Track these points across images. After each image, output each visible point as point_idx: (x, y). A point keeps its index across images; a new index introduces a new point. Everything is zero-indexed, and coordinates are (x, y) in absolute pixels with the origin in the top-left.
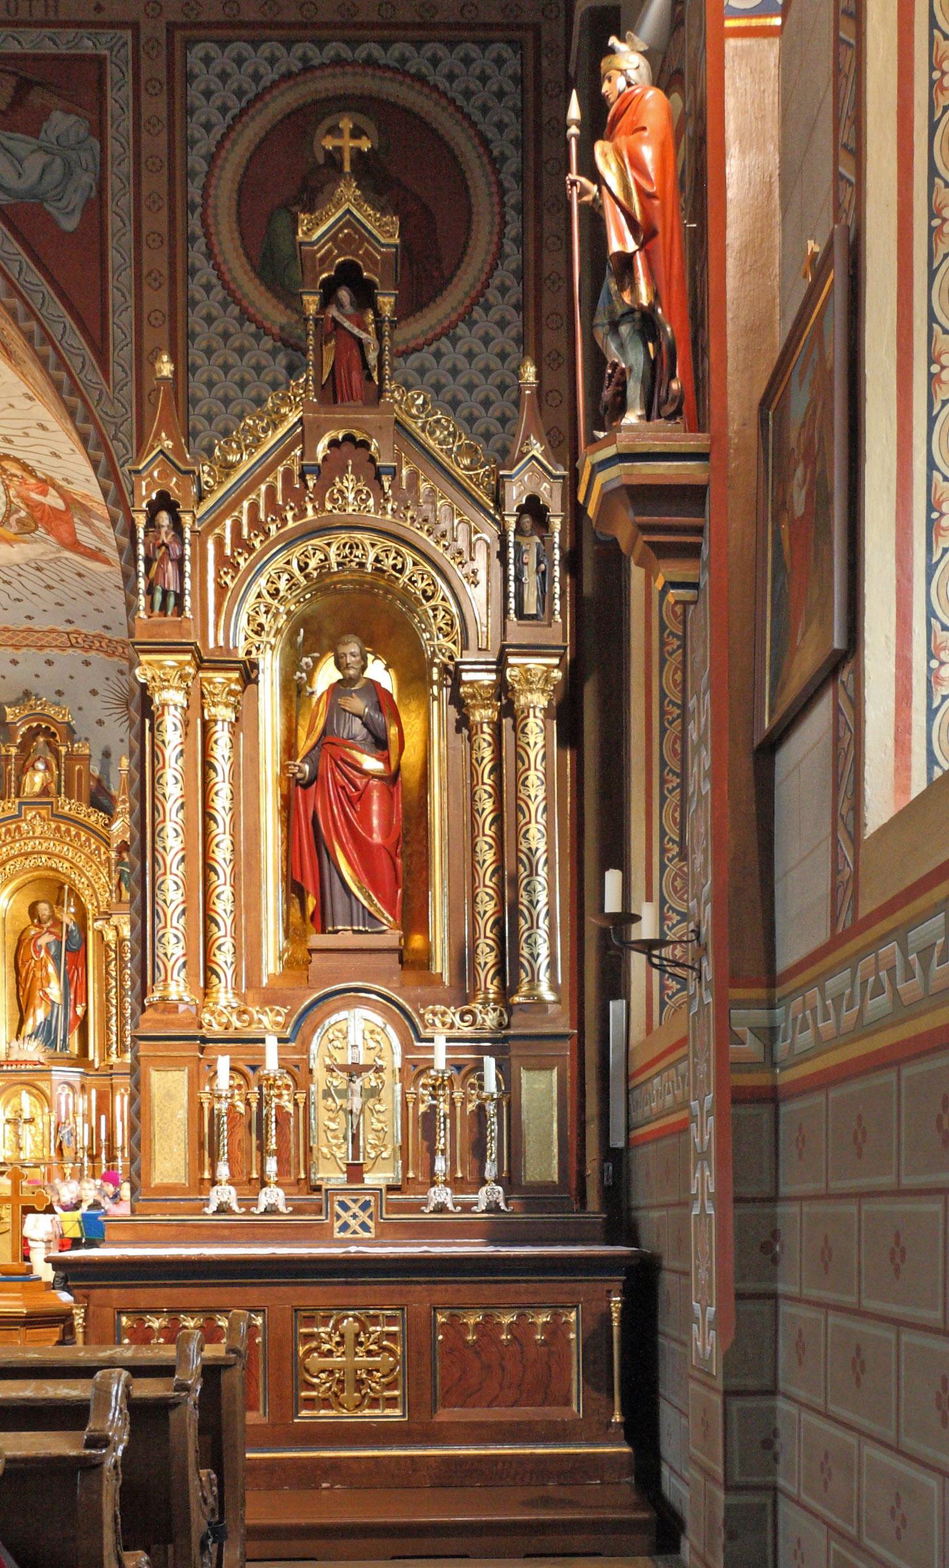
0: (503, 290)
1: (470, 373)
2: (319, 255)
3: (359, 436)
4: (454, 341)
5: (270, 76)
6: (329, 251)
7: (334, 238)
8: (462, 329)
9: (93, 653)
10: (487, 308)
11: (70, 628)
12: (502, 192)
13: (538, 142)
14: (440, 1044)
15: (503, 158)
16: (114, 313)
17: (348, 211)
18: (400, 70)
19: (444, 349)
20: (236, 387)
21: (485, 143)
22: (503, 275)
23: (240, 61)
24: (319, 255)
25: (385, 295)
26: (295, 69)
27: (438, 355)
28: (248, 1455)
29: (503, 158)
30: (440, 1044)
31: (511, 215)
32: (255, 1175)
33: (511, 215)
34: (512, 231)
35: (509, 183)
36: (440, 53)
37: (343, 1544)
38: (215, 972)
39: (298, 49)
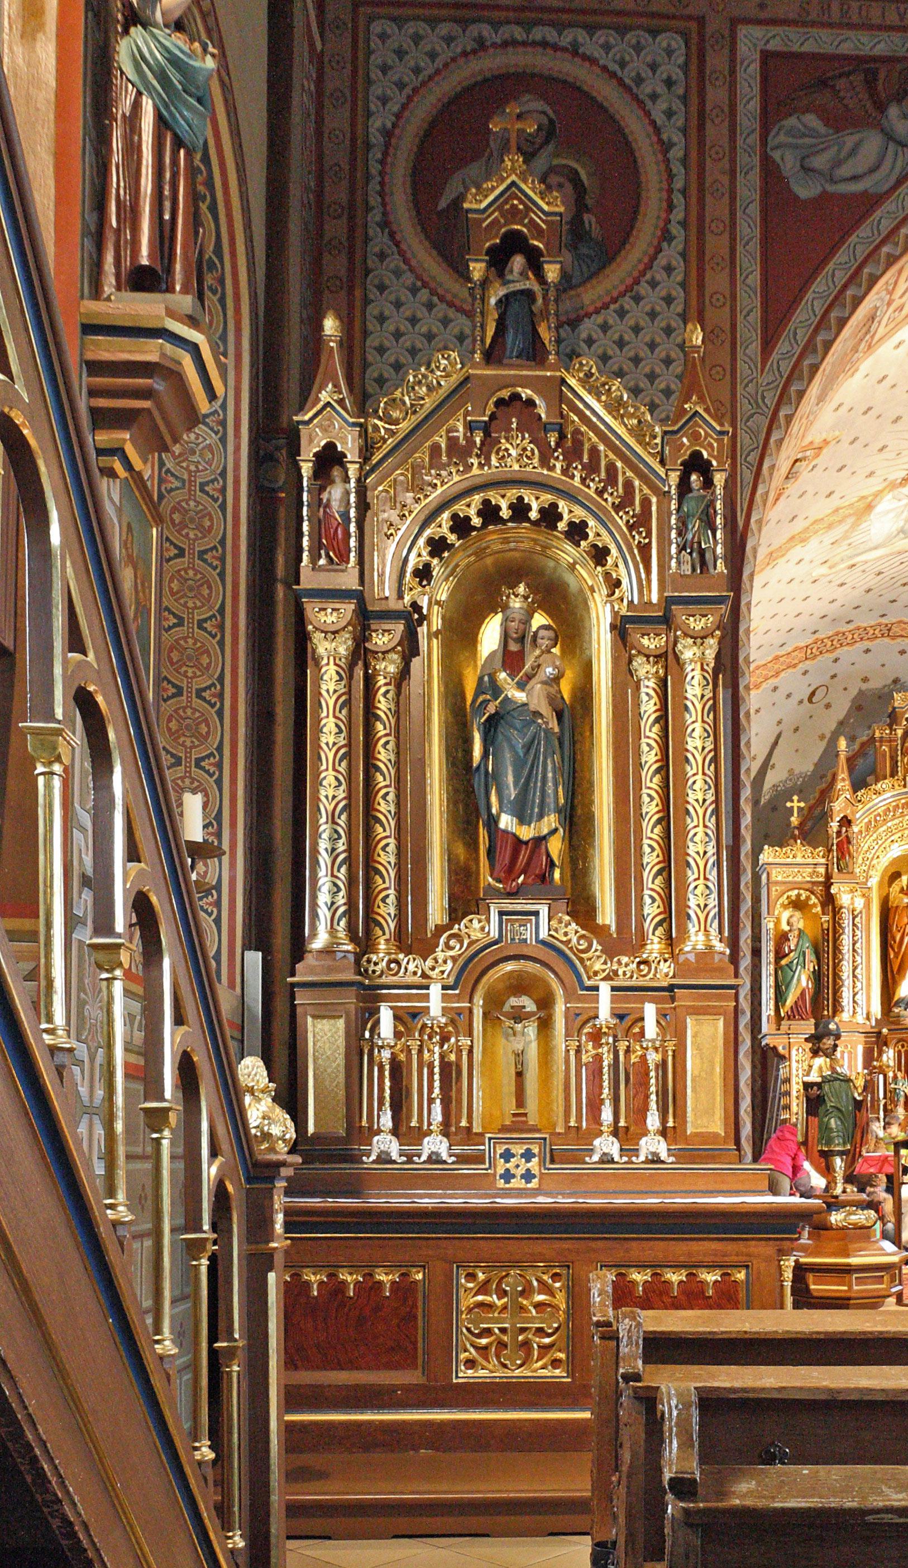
0: (669, 269)
1: (638, 345)
2: (484, 225)
3: (505, 394)
4: (637, 299)
5: (445, 54)
6: (496, 221)
7: (500, 208)
8: (627, 302)
9: (839, 651)
10: (653, 284)
11: (851, 627)
12: (671, 177)
13: (701, 127)
14: (605, 990)
15: (671, 145)
16: (850, 268)
17: (513, 183)
18: (574, 50)
19: (627, 307)
20: (646, 348)
21: (657, 130)
22: (671, 253)
23: (417, 39)
24: (484, 225)
25: (477, 261)
26: (468, 49)
27: (622, 313)
28: (587, 1415)
29: (671, 145)
30: (605, 990)
31: (678, 199)
32: (572, 1124)
33: (678, 199)
34: (678, 215)
35: (677, 168)
36: (611, 40)
37: (221, 1293)
38: (378, 872)
39: (474, 30)
